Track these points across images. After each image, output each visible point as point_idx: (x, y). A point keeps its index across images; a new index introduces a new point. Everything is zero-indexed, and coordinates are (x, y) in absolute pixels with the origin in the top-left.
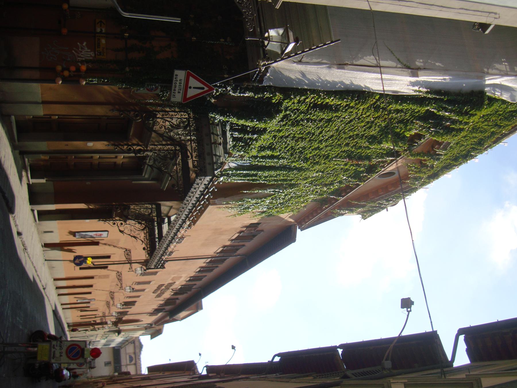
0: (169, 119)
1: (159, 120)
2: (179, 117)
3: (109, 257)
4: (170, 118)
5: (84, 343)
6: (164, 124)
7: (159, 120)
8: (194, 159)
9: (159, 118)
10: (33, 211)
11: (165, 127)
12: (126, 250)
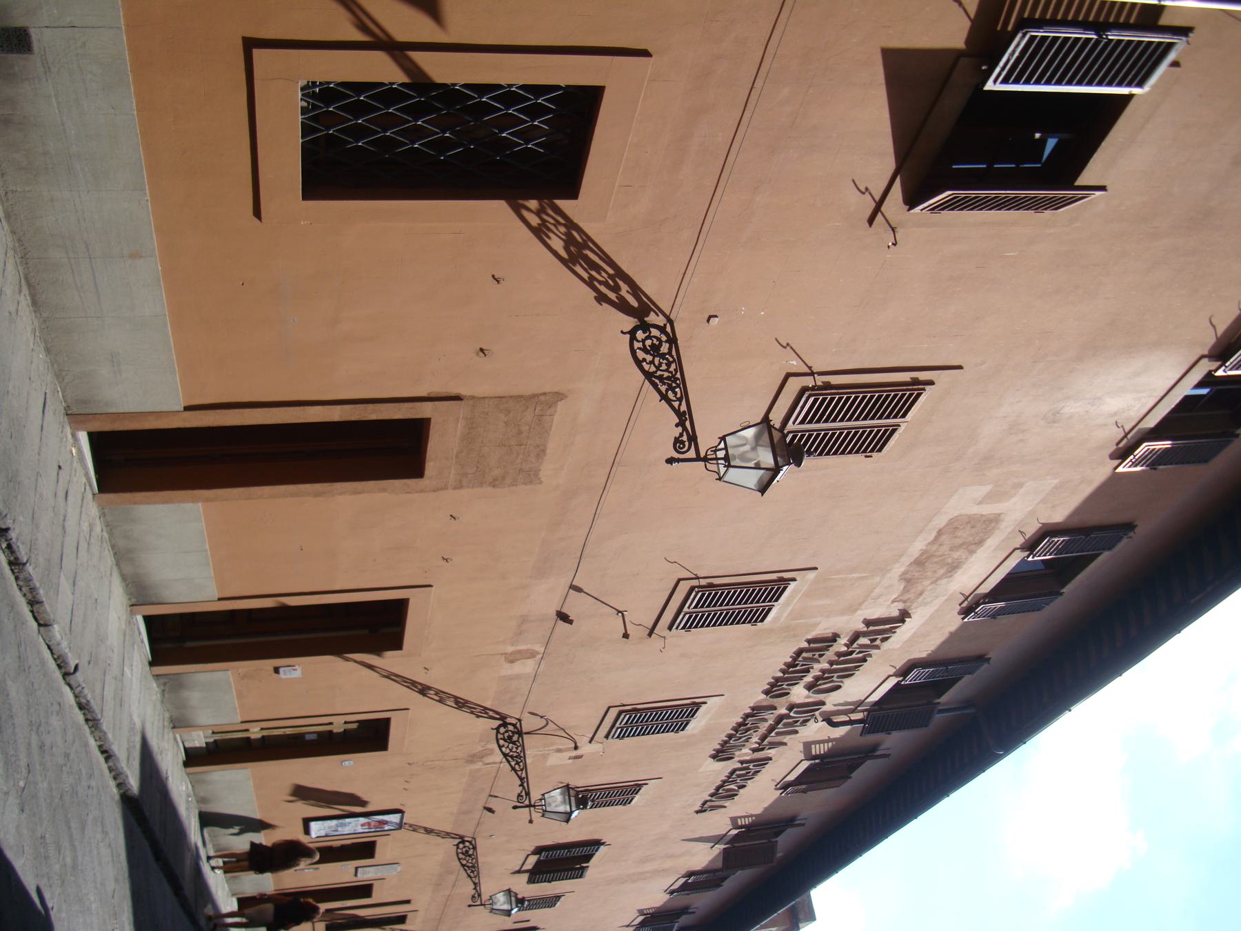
3: (408, 902)
12: (463, 842)
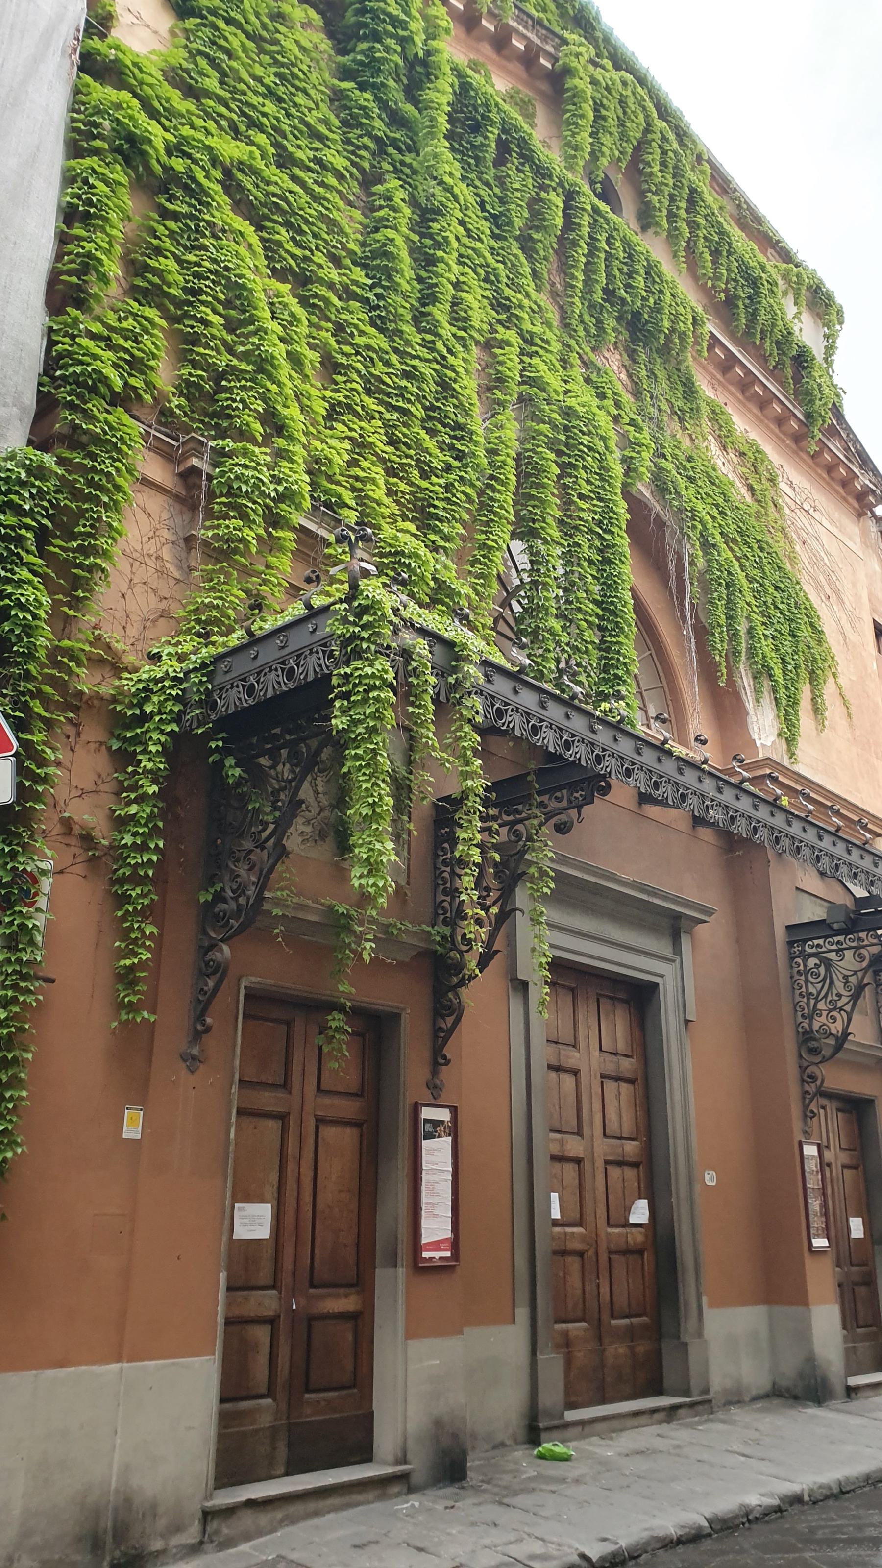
0: (812, 1002)
1: (816, 1027)
2: (803, 977)
4: (808, 999)
5: (323, 1087)
6: (825, 1013)
7: (816, 1027)
8: (565, 803)
9: (810, 1025)
10: (851, 1392)
11: (830, 1011)
